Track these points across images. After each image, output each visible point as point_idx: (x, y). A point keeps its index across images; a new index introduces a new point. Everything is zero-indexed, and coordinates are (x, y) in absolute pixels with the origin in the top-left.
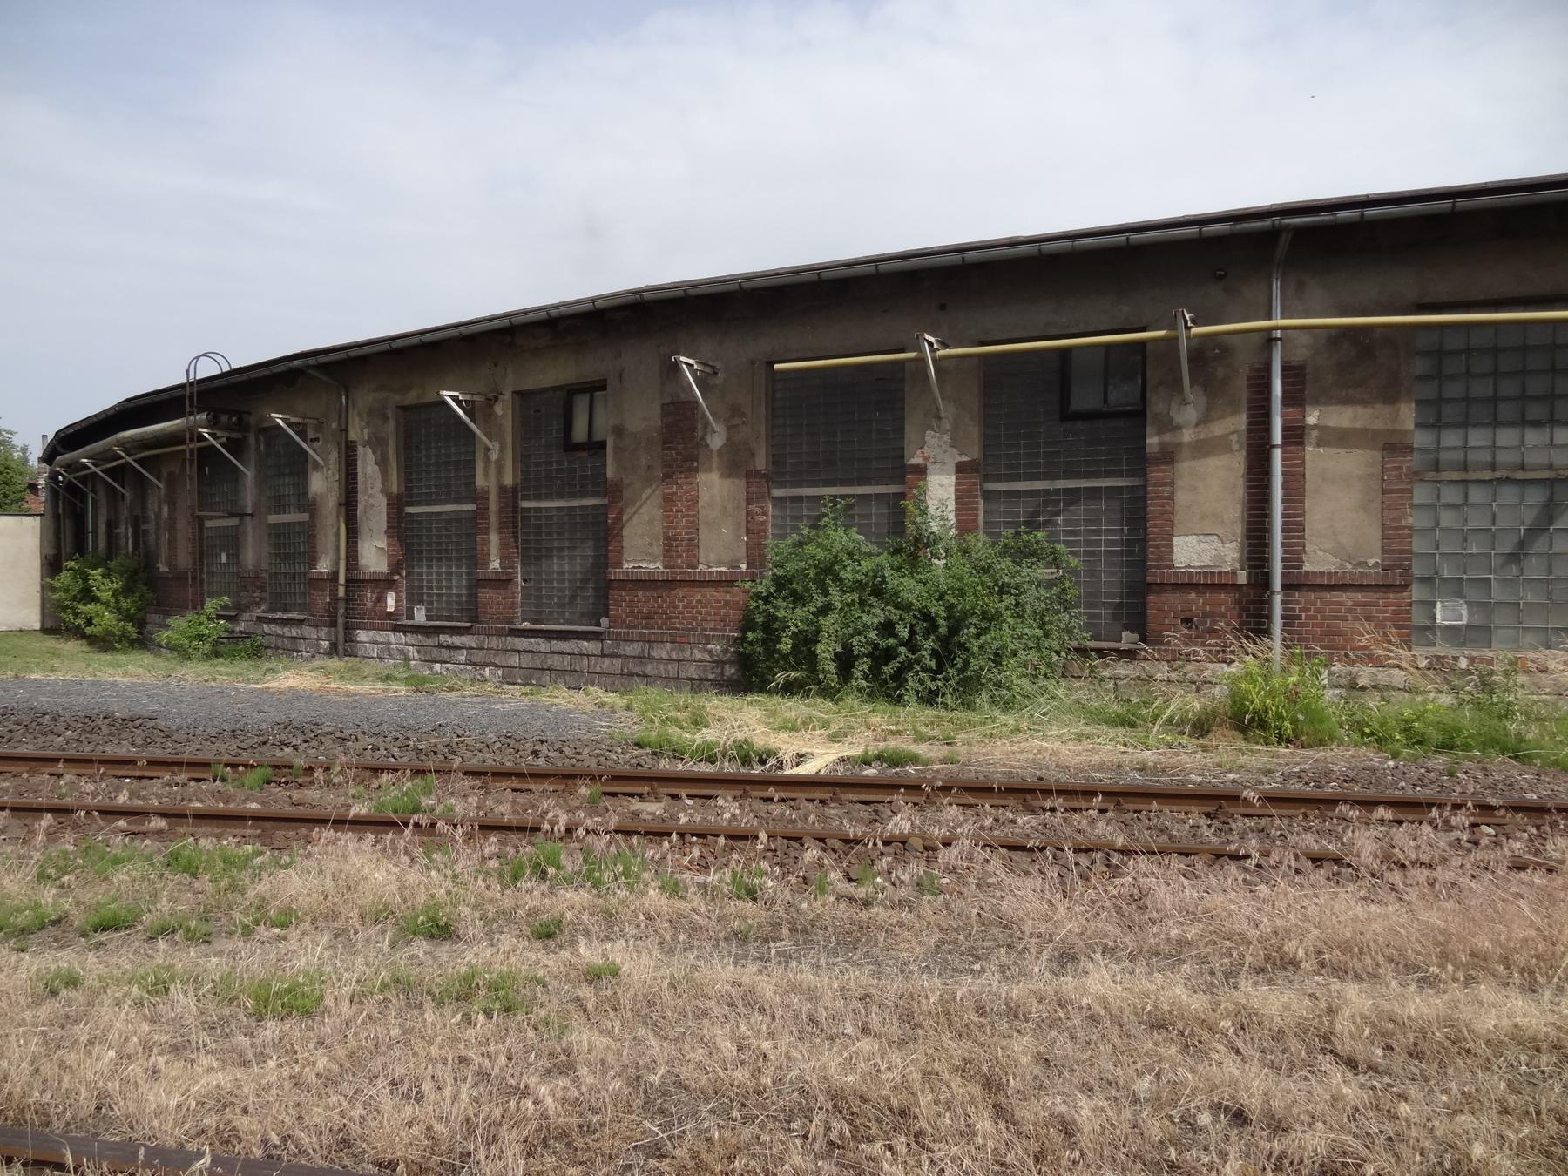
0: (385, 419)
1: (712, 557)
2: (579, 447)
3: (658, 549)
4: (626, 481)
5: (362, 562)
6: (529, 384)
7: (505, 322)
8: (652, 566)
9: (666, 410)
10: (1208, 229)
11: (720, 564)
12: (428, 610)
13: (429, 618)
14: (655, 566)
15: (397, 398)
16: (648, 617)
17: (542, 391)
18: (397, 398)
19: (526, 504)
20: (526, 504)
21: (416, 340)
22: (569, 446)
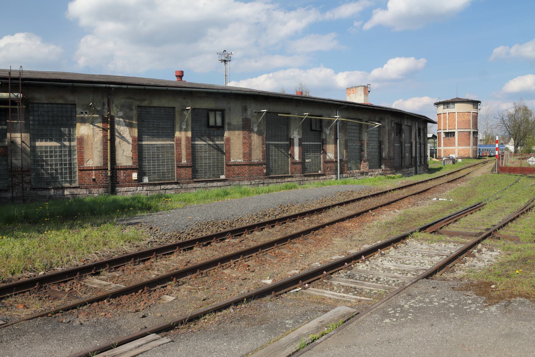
0: (131, 110)
1: (255, 158)
2: (212, 127)
3: (241, 156)
4: (231, 138)
5: (118, 162)
6: (198, 106)
7: (291, 97)
8: (240, 161)
9: (243, 120)
10: (129, 86)
11: (257, 159)
12: (149, 178)
13: (149, 181)
14: (240, 160)
15: (138, 103)
16: (239, 174)
17: (198, 109)
18: (138, 103)
19: (288, 143)
20: (288, 143)
21: (312, 100)
22: (208, 126)
